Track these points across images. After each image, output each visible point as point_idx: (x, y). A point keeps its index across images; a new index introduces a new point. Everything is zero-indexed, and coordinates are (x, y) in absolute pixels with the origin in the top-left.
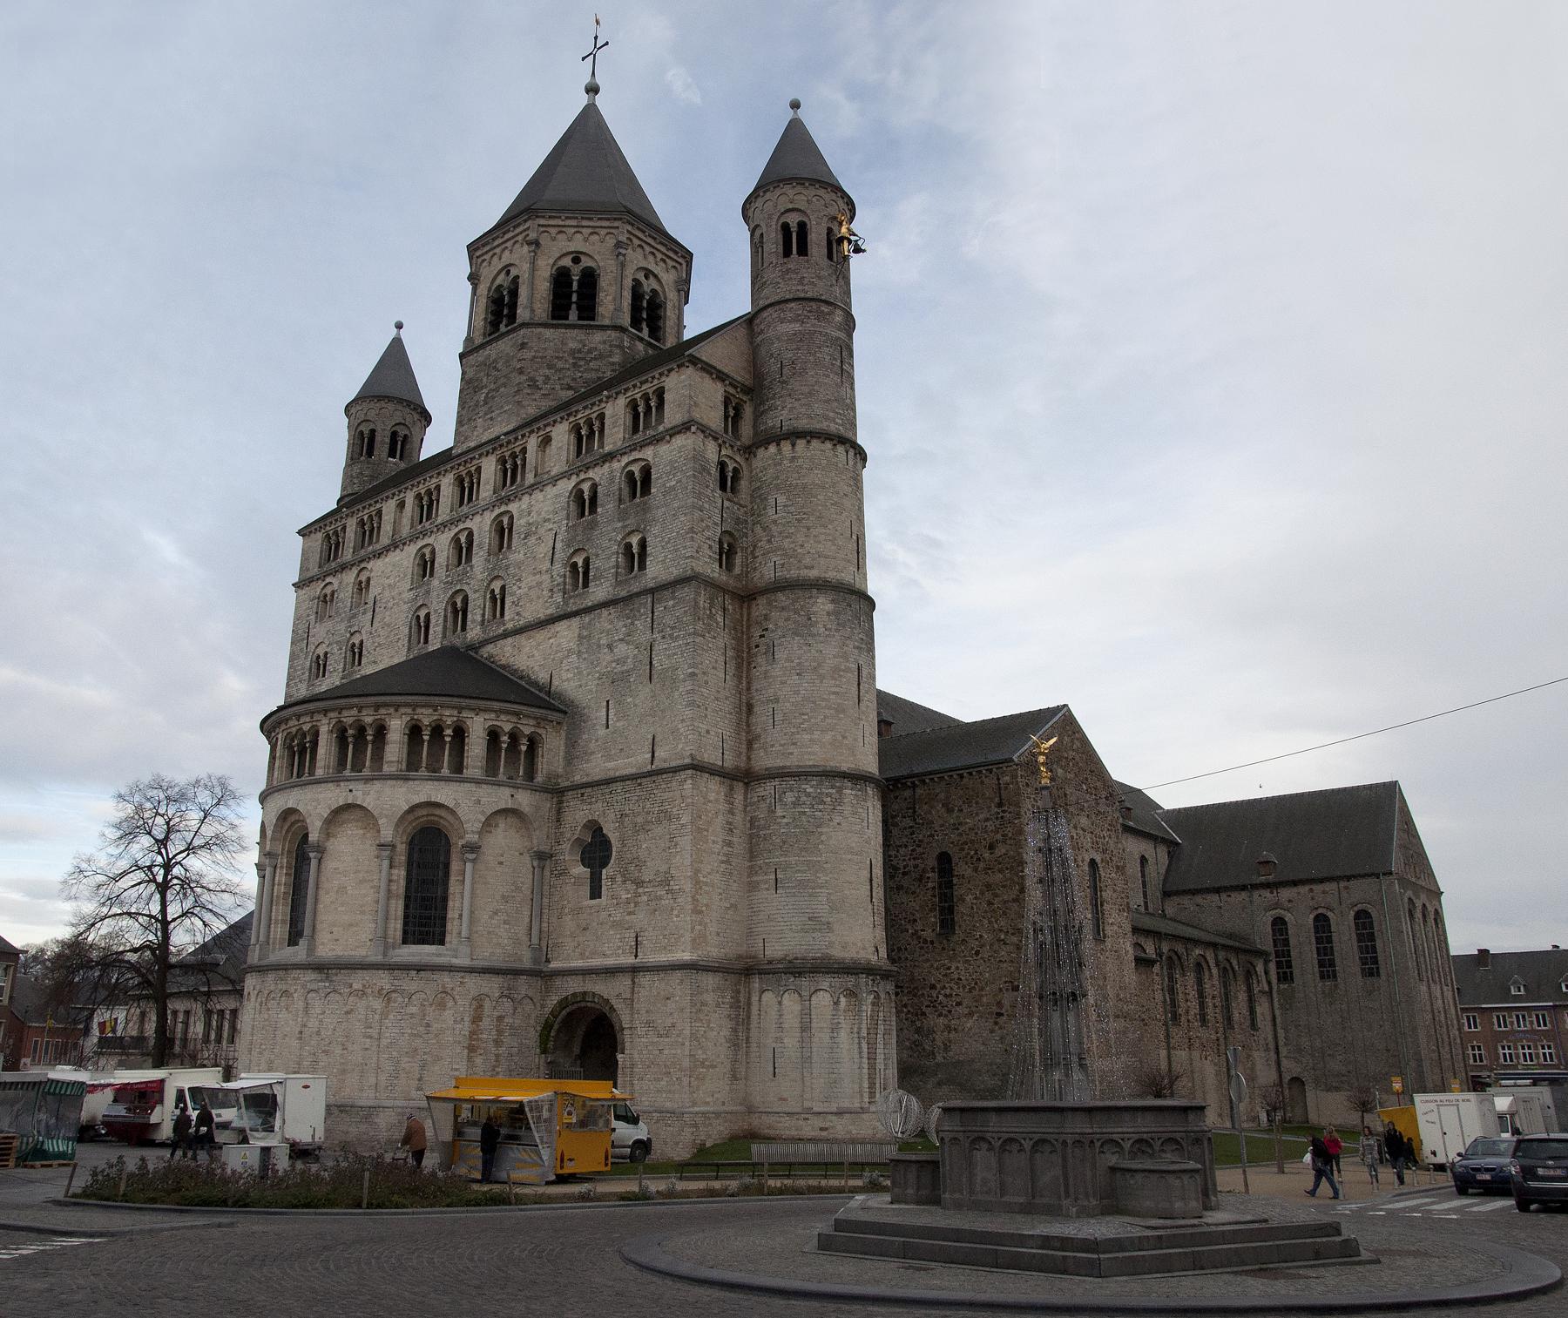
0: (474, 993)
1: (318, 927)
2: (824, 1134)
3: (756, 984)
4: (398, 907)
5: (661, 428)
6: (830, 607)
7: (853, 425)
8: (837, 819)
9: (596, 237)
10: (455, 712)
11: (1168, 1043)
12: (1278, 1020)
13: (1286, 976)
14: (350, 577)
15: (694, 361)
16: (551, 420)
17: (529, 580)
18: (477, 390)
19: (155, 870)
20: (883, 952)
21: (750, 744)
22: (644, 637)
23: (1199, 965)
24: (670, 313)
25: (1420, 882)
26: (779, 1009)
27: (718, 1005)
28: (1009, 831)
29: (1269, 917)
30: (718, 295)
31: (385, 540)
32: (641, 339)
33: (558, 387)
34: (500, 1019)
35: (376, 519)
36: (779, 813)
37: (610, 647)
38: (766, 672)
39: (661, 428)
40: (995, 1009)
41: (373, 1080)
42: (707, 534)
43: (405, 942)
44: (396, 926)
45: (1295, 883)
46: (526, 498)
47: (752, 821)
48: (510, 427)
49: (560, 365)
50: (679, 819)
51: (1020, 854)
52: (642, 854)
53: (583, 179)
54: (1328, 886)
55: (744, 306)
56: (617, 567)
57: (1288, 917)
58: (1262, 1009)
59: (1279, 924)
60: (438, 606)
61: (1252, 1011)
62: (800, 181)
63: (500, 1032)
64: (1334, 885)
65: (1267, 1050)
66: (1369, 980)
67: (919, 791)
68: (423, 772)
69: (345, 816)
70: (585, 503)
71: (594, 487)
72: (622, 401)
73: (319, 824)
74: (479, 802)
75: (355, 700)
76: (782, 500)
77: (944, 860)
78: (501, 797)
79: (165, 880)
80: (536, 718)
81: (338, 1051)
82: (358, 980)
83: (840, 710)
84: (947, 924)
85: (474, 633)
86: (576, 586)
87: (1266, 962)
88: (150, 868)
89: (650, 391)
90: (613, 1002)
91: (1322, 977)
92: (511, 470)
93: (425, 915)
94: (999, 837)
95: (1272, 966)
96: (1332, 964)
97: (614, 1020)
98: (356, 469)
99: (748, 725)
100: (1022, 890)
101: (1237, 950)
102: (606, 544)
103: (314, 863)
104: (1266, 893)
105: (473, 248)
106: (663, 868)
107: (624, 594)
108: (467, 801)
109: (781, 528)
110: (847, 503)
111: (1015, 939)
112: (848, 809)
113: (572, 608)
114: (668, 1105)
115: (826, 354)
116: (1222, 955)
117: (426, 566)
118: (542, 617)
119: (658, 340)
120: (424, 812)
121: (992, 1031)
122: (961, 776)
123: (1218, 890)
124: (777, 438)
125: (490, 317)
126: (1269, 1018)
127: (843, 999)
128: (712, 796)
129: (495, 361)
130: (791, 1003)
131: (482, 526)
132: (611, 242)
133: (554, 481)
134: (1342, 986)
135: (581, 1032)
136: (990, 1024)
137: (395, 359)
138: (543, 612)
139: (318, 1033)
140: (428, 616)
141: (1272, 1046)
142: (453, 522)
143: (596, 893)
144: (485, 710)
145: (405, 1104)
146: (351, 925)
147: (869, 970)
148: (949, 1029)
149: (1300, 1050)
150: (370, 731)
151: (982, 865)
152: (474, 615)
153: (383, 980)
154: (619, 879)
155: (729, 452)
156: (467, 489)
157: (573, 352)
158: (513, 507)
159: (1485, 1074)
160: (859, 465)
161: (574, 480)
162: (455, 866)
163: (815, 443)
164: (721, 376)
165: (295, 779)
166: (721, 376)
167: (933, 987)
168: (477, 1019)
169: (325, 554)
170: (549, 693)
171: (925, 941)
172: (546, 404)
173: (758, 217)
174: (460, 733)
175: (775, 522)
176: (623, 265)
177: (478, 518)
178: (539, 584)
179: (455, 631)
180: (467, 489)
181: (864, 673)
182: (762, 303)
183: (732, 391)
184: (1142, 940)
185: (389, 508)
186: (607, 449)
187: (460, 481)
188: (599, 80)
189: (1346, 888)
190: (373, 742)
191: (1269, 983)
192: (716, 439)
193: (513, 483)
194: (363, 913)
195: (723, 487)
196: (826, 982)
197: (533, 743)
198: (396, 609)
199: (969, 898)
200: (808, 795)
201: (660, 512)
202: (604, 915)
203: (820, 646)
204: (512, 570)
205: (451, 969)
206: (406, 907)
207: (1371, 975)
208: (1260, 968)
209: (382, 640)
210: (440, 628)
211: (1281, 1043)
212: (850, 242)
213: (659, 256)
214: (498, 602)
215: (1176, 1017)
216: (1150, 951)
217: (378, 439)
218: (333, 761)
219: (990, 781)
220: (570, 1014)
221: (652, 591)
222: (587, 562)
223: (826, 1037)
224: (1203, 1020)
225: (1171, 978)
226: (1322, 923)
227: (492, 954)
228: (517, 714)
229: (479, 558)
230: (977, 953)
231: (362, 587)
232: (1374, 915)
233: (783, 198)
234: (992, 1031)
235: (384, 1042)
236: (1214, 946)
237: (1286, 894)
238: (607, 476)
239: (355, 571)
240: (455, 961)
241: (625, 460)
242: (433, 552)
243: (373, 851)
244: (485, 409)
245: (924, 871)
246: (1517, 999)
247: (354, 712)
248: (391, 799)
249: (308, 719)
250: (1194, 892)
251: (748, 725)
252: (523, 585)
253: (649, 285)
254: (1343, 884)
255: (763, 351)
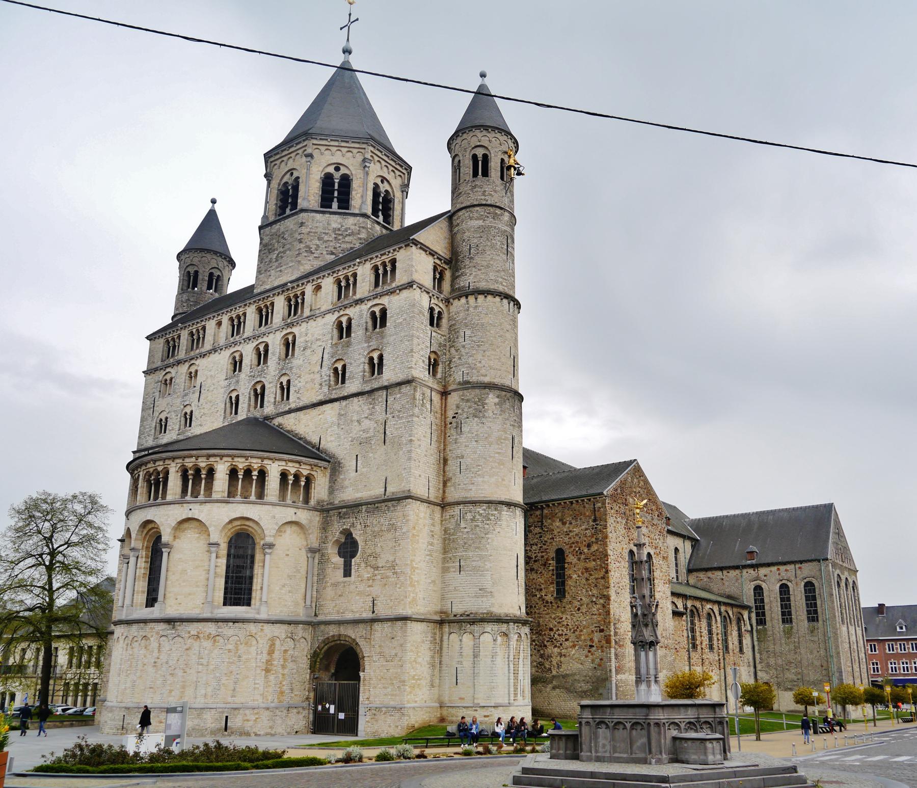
0: (269, 636)
1: (168, 595)
2: (486, 719)
3: (446, 629)
4: (221, 583)
5: (394, 285)
6: (497, 400)
7: (513, 287)
8: (498, 530)
9: (350, 154)
10: (259, 461)
11: (690, 662)
12: (756, 648)
13: (761, 621)
14: (183, 369)
15: (416, 243)
16: (321, 275)
17: (306, 377)
18: (270, 251)
19: (44, 556)
20: (523, 610)
21: (445, 484)
22: (381, 417)
23: (709, 614)
24: (397, 207)
25: (844, 565)
26: (460, 643)
27: (423, 642)
28: (600, 536)
29: (752, 585)
30: (427, 196)
31: (208, 346)
32: (378, 223)
33: (325, 252)
34: (286, 651)
35: (201, 332)
36: (463, 525)
37: (358, 421)
38: (456, 439)
39: (394, 285)
40: (589, 643)
41: (203, 692)
42: (422, 353)
43: (225, 604)
44: (220, 595)
45: (769, 565)
46: (304, 324)
47: (445, 531)
48: (293, 278)
49: (326, 238)
50: (401, 529)
51: (606, 551)
52: (378, 550)
53: (340, 107)
54: (788, 567)
55: (446, 206)
56: (364, 372)
57: (764, 585)
58: (747, 641)
59: (758, 590)
60: (245, 391)
61: (741, 642)
62: (486, 128)
63: (285, 660)
64: (792, 566)
65: (749, 666)
66: (812, 624)
67: (545, 511)
68: (238, 498)
69: (186, 525)
70: (344, 330)
71: (350, 321)
72: (368, 266)
73: (169, 530)
74: (274, 517)
75: (194, 452)
76: (468, 333)
77: (560, 553)
78: (289, 514)
79: (52, 562)
80: (311, 465)
81: (180, 673)
82: (193, 628)
83: (501, 463)
84: (561, 593)
85: (269, 409)
86: (337, 382)
87: (750, 613)
88: (41, 555)
89: (387, 261)
90: (358, 640)
91: (783, 621)
92: (295, 305)
93: (238, 589)
94: (594, 540)
95: (753, 615)
96: (790, 613)
97: (358, 651)
98: (185, 297)
99: (444, 472)
100: (607, 572)
101: (732, 605)
102: (357, 357)
103: (165, 555)
104: (751, 571)
105: (268, 156)
106: (391, 558)
107: (368, 389)
108: (269, 516)
109: (467, 350)
110: (508, 335)
111: (602, 601)
112: (504, 523)
113: (334, 396)
114: (392, 703)
115: (498, 241)
116: (723, 608)
117: (237, 365)
118: (315, 401)
119: (389, 224)
120: (238, 523)
121: (587, 656)
122: (572, 503)
123: (721, 569)
124: (466, 293)
125: (279, 203)
126: (750, 646)
127: (499, 638)
128: (422, 515)
129: (283, 233)
130: (467, 639)
131: (275, 341)
132: (360, 158)
133: (324, 314)
134: (795, 628)
135: (335, 658)
136: (586, 652)
137: (211, 222)
138: (315, 399)
139: (167, 663)
140: (237, 397)
141: (752, 664)
142: (255, 337)
143: (347, 573)
144: (279, 460)
145: (224, 706)
146: (190, 594)
147: (516, 621)
148: (561, 655)
149: (768, 665)
150: (204, 472)
151: (583, 557)
152: (269, 398)
153: (211, 628)
154: (363, 565)
155: (436, 301)
156: (264, 316)
157: (335, 230)
158: (295, 330)
159: (880, 679)
160: (516, 312)
161: (336, 315)
162: (258, 557)
163: (490, 297)
164: (432, 253)
165: (152, 501)
166: (432, 253)
167: (551, 629)
168: (271, 652)
169: (166, 354)
170: (318, 449)
171: (547, 602)
172: (318, 264)
173: (457, 149)
174: (262, 474)
175: (464, 346)
176: (367, 174)
177: (271, 336)
178: (313, 380)
179: (256, 407)
180: (264, 316)
181: (516, 441)
182: (458, 206)
183: (438, 262)
184: (675, 600)
185: (211, 325)
186: (358, 296)
187: (260, 310)
188: (352, 45)
189: (800, 568)
190: (206, 479)
191: (751, 625)
192: (428, 293)
193: (295, 315)
194: (198, 586)
195: (432, 324)
196: (489, 627)
197: (309, 480)
198: (215, 391)
199: (575, 576)
200: (481, 515)
201: (392, 338)
202: (353, 587)
203: (489, 424)
204: (294, 370)
205: (255, 621)
206: (226, 582)
207: (813, 621)
208: (746, 616)
209: (206, 411)
210: (246, 405)
211: (757, 662)
212: (515, 169)
213: (391, 168)
214: (285, 390)
215: (694, 646)
216: (681, 608)
217: (200, 277)
218: (179, 489)
219: (589, 506)
220: (329, 648)
221: (386, 388)
222: (344, 367)
223: (489, 660)
224: (711, 647)
225: (692, 623)
226: (784, 589)
227: (281, 612)
228: (299, 462)
229: (273, 360)
230: (579, 609)
231: (192, 376)
232: (816, 585)
233: (474, 138)
234: (587, 656)
235: (211, 667)
236: (719, 603)
237: (763, 571)
238: (359, 314)
239: (187, 365)
240: (258, 617)
241: (370, 304)
242: (241, 356)
243: (205, 547)
244: (276, 264)
245: (547, 559)
246: (901, 633)
247: (193, 459)
248: (218, 514)
249: (161, 463)
250: (706, 570)
251: (444, 472)
252: (302, 380)
253: (384, 187)
254: (798, 566)
255: (459, 236)
